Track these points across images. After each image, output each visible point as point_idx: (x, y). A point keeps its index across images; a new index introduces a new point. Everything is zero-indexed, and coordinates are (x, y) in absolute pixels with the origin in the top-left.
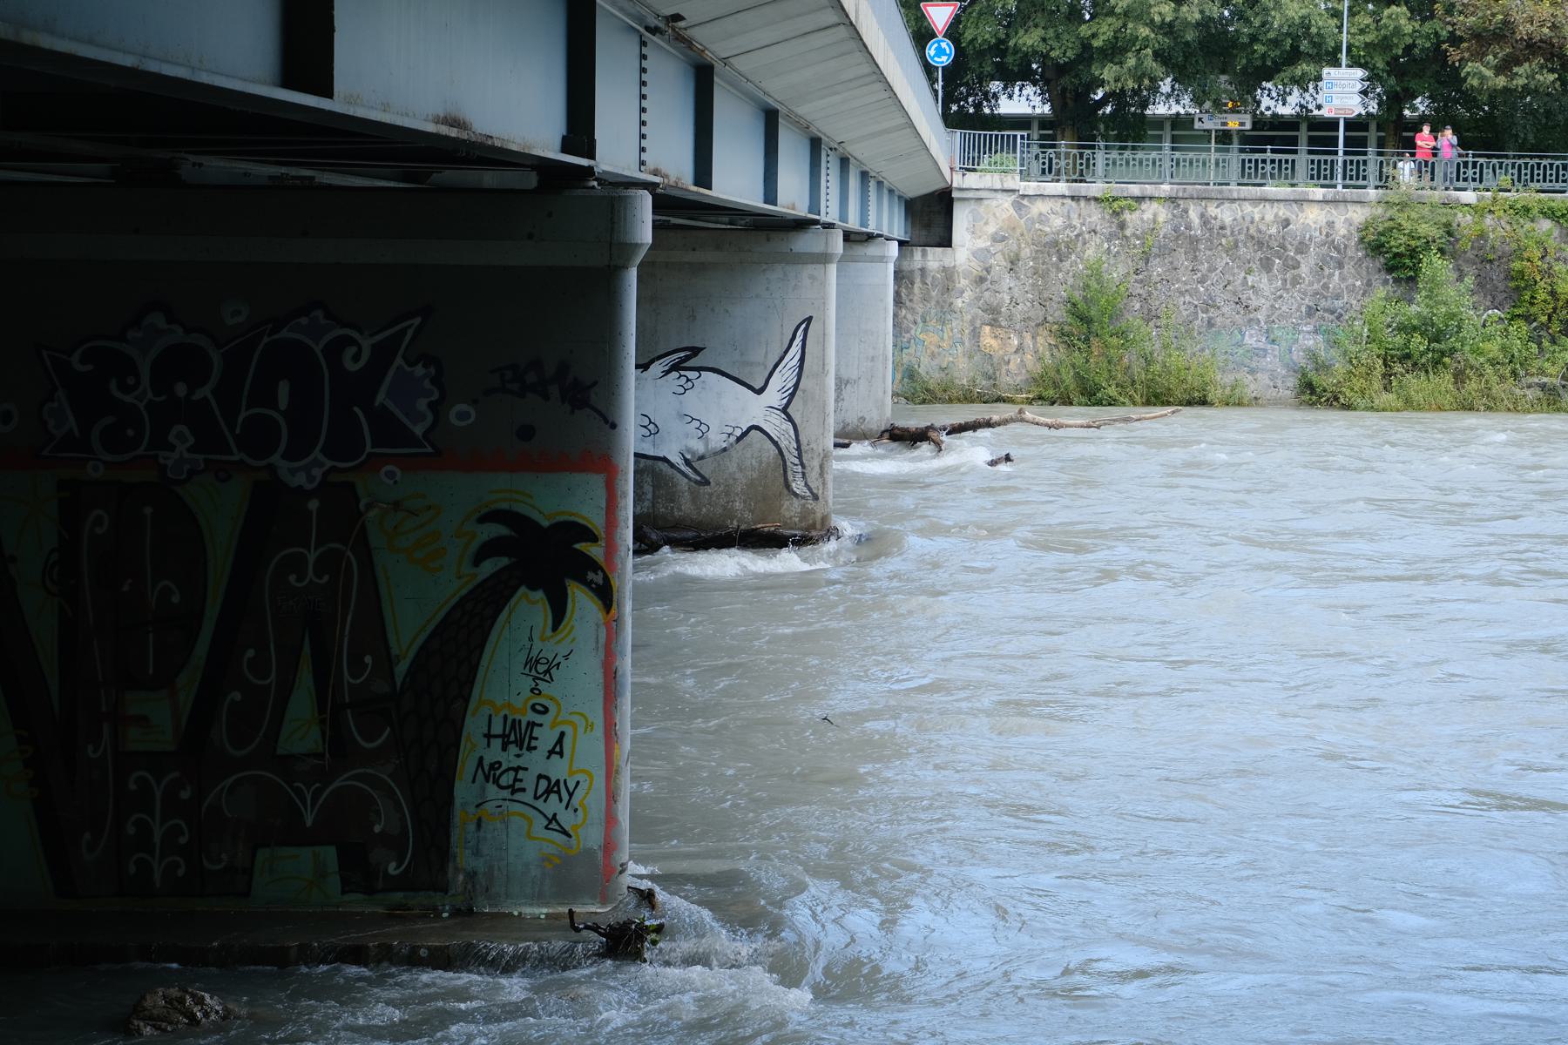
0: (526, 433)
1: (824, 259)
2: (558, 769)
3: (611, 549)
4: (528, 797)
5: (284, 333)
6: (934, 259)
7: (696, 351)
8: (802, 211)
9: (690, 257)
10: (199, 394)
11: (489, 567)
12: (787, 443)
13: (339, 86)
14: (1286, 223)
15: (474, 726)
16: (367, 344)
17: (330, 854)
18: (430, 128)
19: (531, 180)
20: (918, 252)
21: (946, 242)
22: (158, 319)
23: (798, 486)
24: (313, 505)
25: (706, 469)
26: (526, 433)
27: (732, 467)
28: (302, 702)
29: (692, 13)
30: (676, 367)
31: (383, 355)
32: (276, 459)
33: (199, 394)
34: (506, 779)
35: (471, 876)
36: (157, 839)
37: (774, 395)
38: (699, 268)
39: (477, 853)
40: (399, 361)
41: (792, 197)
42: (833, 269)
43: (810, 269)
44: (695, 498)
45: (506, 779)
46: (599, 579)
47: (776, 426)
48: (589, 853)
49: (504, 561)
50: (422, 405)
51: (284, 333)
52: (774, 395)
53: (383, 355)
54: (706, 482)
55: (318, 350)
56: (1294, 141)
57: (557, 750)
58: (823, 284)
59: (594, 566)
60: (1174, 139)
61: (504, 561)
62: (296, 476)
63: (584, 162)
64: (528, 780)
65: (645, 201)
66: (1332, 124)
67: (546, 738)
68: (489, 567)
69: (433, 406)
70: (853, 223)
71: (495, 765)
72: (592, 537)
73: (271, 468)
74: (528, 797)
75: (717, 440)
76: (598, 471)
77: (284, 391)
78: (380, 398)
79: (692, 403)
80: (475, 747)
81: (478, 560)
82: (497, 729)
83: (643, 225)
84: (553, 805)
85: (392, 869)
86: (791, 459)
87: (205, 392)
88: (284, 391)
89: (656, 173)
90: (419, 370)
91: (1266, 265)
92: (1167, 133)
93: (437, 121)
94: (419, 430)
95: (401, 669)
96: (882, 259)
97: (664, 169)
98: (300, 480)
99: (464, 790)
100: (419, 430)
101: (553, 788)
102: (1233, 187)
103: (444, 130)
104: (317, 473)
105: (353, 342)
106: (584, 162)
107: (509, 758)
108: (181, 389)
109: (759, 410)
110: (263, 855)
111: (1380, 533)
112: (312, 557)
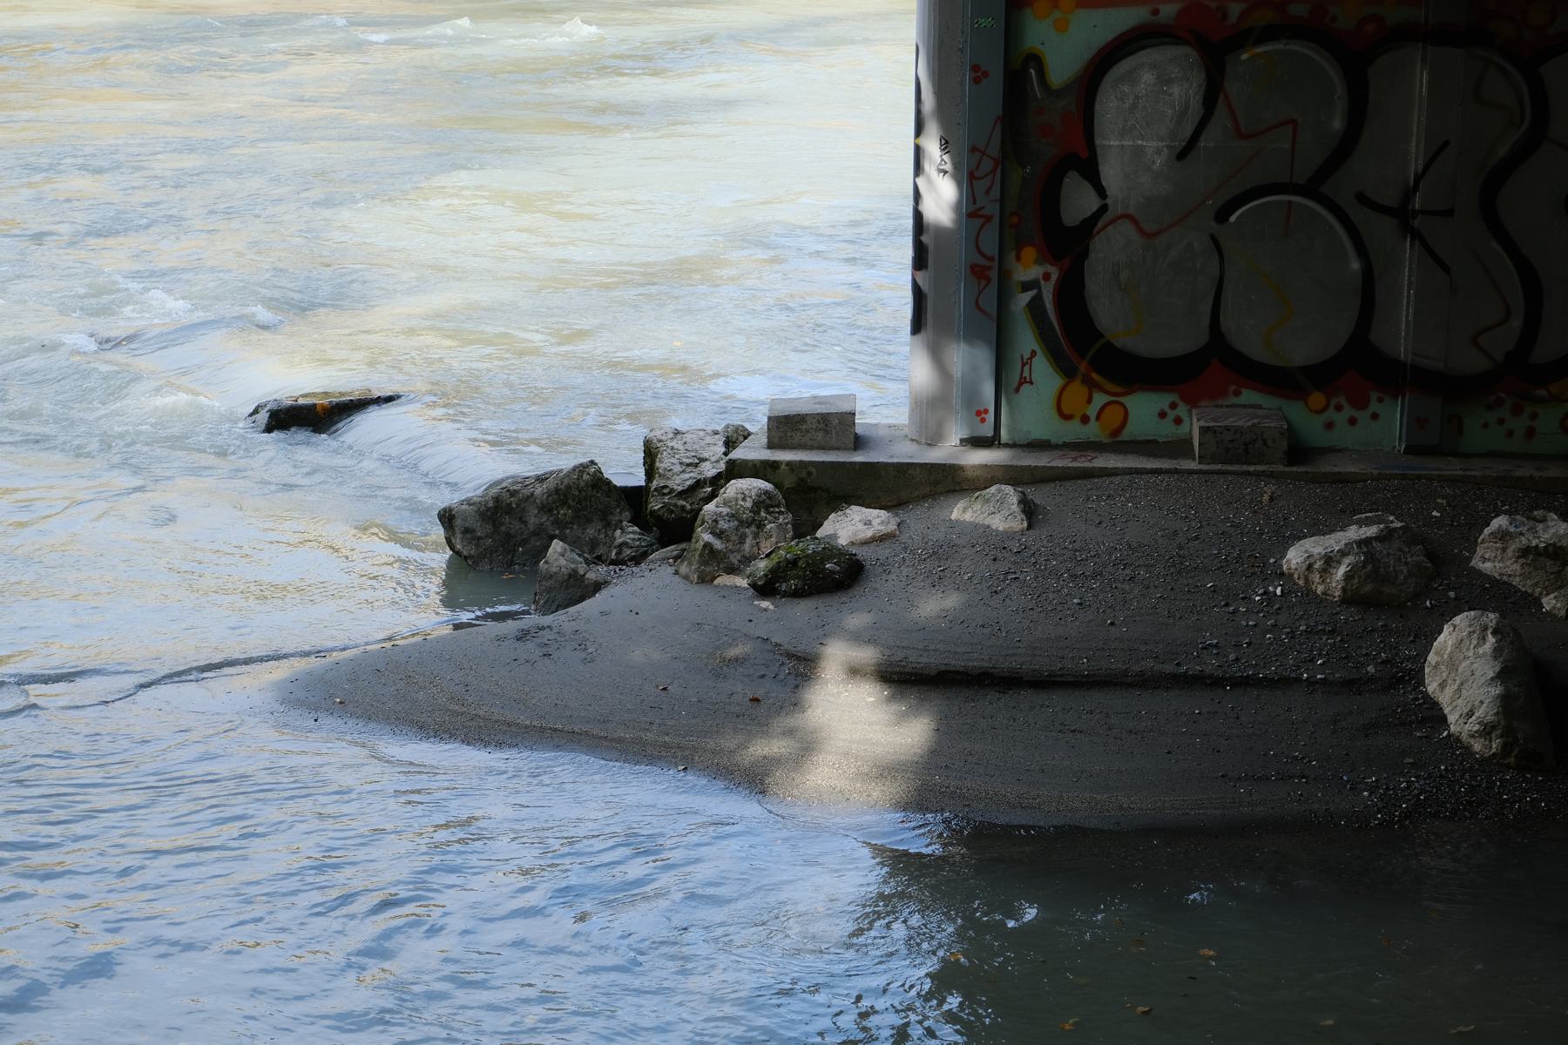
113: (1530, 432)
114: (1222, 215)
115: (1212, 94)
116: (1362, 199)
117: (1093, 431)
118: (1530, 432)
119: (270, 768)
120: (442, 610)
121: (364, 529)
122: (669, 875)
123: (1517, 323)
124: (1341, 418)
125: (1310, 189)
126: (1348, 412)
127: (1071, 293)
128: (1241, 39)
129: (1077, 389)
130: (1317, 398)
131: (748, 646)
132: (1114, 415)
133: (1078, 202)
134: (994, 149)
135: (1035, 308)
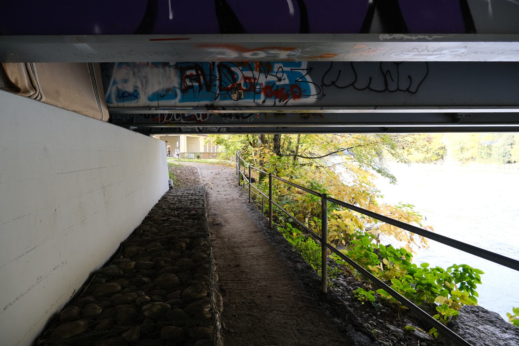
38: (94, 83)
61: (304, 50)
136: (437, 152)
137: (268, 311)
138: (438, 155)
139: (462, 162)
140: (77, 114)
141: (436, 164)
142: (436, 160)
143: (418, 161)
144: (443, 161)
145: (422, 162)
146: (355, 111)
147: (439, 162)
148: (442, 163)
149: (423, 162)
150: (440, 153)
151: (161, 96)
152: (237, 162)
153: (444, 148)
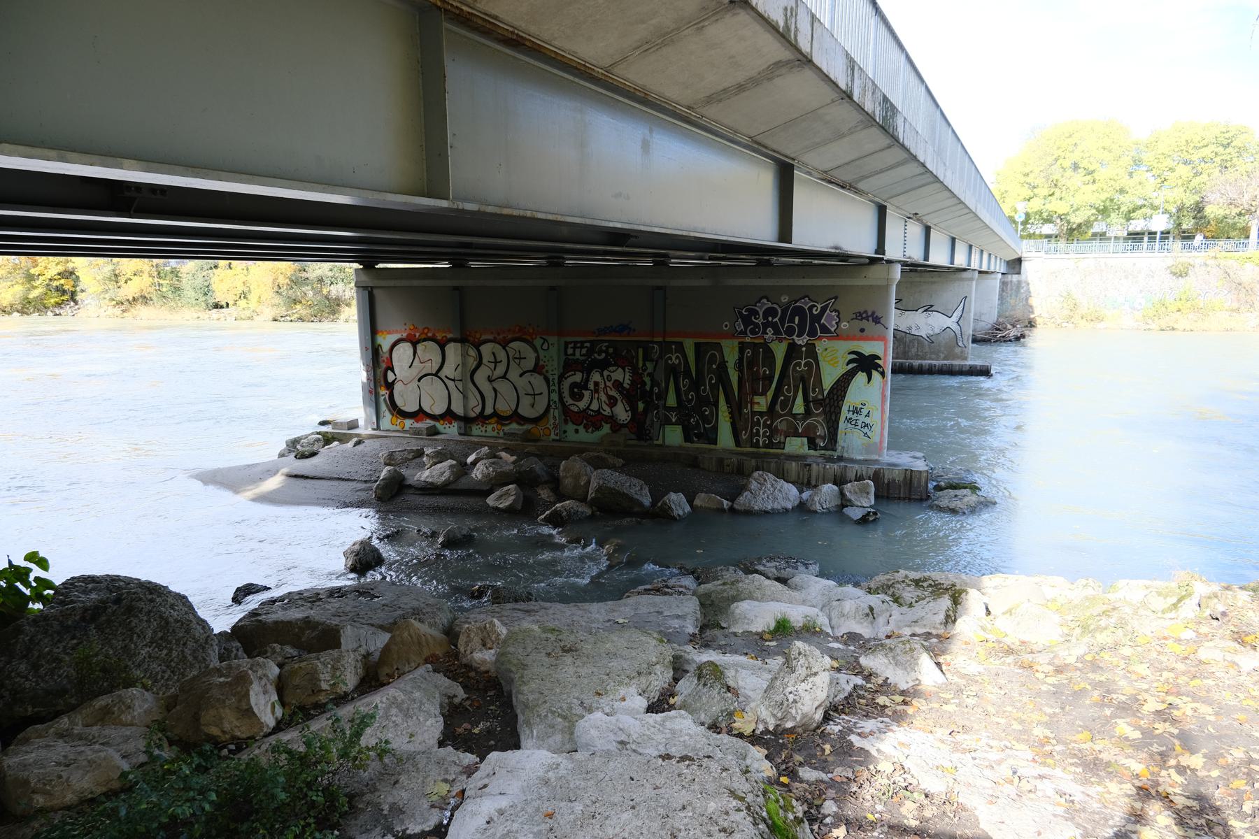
0: (862, 330)
1: (972, 279)
2: (867, 420)
3: (885, 362)
4: (859, 427)
5: (797, 304)
6: (1015, 278)
7: (932, 306)
8: (964, 266)
9: (932, 280)
10: (775, 320)
11: (851, 366)
12: (958, 332)
13: (794, 241)
14: (1134, 264)
15: (845, 408)
16: (819, 307)
17: (805, 440)
18: (826, 250)
19: (867, 261)
20: (1009, 276)
21: (1019, 273)
22: (765, 301)
23: (960, 344)
24: (804, 349)
25: (933, 339)
26: (862, 330)
27: (941, 339)
28: (799, 400)
29: (921, 213)
30: (925, 311)
31: (824, 310)
32: (794, 337)
33: (775, 320)
34: (853, 423)
35: (843, 447)
36: (761, 433)
37: (955, 318)
38: (933, 283)
39: (845, 441)
40: (828, 311)
41: (960, 261)
42: (974, 283)
43: (967, 282)
44: (929, 347)
45: (853, 423)
46: (881, 370)
47: (955, 327)
48: (876, 443)
49: (855, 365)
50: (834, 323)
51: (797, 304)
52: (955, 318)
53: (824, 310)
54: (933, 342)
55: (806, 308)
56: (1142, 239)
57: (868, 415)
58: (971, 287)
59: (880, 366)
60: (1101, 239)
61: (855, 365)
62: (801, 341)
63: (881, 256)
64: (859, 423)
65: (898, 268)
66: (1155, 233)
67: (865, 412)
68: (851, 366)
69: (837, 323)
70: (984, 268)
71: (850, 419)
72: (879, 358)
73: (793, 339)
74: (859, 427)
75: (937, 331)
76: (882, 340)
77: (797, 318)
78: (822, 321)
79: (930, 320)
80: (844, 413)
81: (848, 364)
82: (851, 409)
83: (897, 272)
84: (866, 430)
85: (822, 444)
86: (959, 336)
87: (776, 319)
88: (797, 318)
89: (910, 258)
90: (833, 314)
91: (1126, 277)
92: (1098, 237)
93: (831, 248)
94: (833, 330)
95: (826, 393)
96: (996, 279)
97: (912, 256)
98: (800, 342)
99: (842, 425)
100: (833, 330)
101: (866, 425)
102: (1144, 253)
103: (834, 251)
104: (805, 341)
105: (816, 306)
106: (881, 256)
107: (854, 417)
108: (770, 319)
109: (951, 323)
110: (788, 439)
111: (130, 450)
112: (803, 363)
113: (486, 431)
114: (419, 380)
115: (415, 353)
116: (446, 377)
117: (398, 428)
118: (486, 431)
119: (43, 491)
120: (874, 753)
121: (397, 532)
122: (399, 501)
123: (480, 406)
124: (447, 426)
125: (436, 375)
126: (448, 425)
127: (391, 396)
128: (419, 342)
129: (394, 418)
130: (442, 422)
131: (492, 651)
132: (402, 424)
133: (391, 377)
134: (371, 365)
135: (385, 400)
136: (55, 284)
137: (804, 785)
138: (60, 290)
139: (123, 307)
140: (363, 376)
141: (60, 314)
142: (58, 305)
143: (8, 309)
144: (77, 307)
145: (18, 311)
146: (60, 169)
147: (67, 310)
148: (75, 312)
149: (23, 312)
150: (66, 287)
151: (946, 602)
152: (627, 411)
153: (72, 273)
